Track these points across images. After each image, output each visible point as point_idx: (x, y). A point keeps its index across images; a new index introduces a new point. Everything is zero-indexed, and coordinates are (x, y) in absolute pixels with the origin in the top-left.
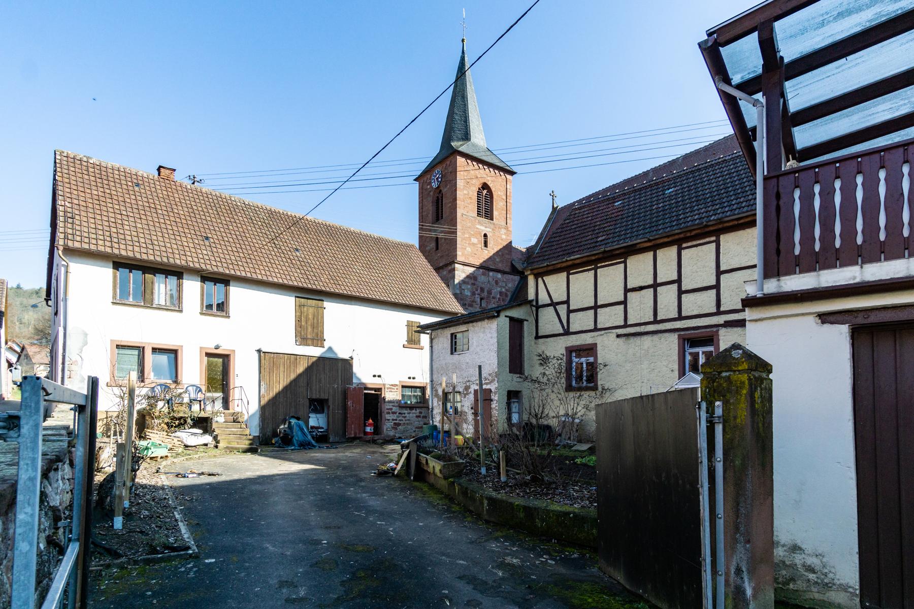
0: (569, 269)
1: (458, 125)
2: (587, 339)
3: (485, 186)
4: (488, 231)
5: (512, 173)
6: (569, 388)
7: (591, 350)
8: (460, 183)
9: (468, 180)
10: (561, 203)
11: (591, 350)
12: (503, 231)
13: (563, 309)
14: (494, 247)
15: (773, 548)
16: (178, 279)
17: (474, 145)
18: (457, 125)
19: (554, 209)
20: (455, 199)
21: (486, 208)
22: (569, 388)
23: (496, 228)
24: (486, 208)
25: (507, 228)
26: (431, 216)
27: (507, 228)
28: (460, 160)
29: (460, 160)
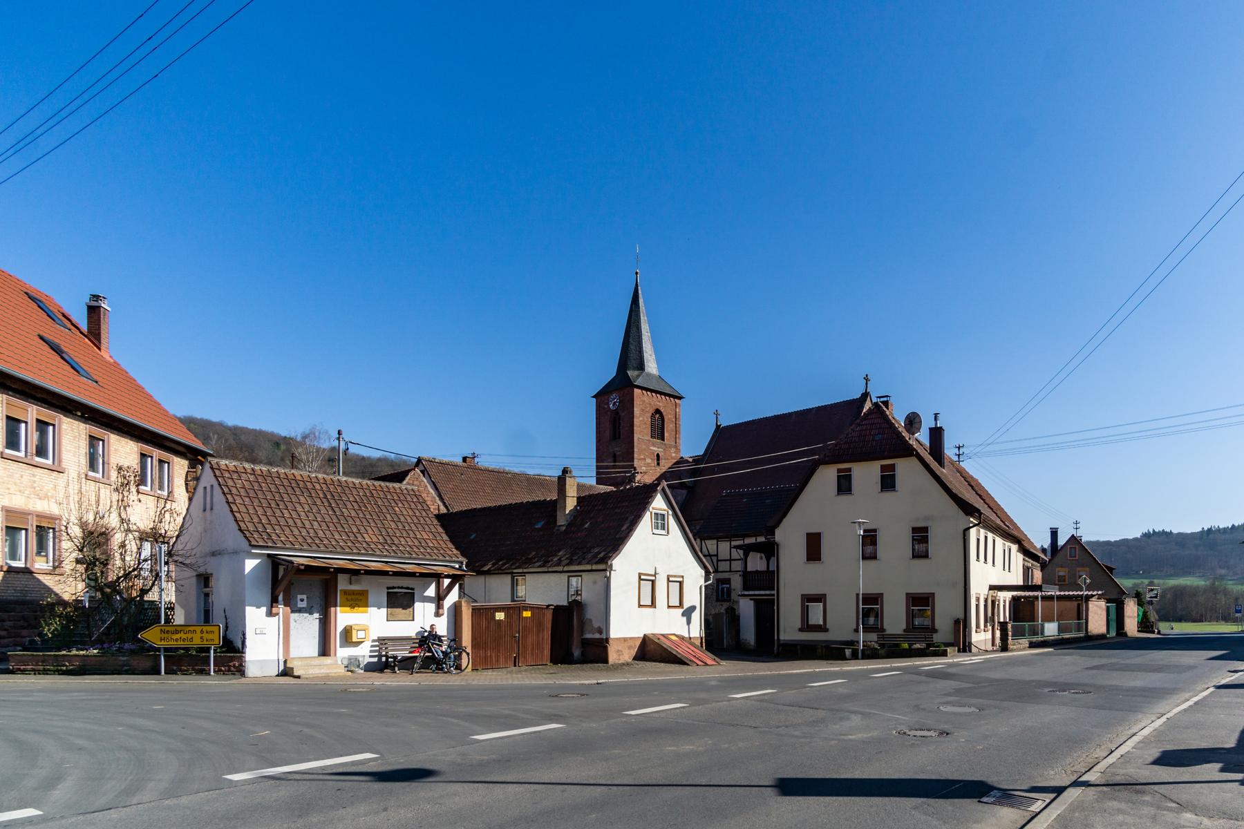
0: (718, 539)
1: (633, 355)
2: (726, 575)
3: (658, 411)
4: (660, 450)
5: (680, 398)
6: (717, 600)
7: (728, 581)
8: (637, 411)
9: (643, 405)
10: (724, 423)
11: (728, 581)
12: (673, 450)
13: (714, 559)
14: (665, 465)
15: (476, 469)
17: (649, 375)
18: (630, 355)
19: (718, 427)
20: (632, 425)
21: (658, 431)
22: (717, 600)
23: (666, 447)
24: (658, 431)
25: (676, 447)
26: (608, 434)
27: (676, 447)
28: (637, 391)
29: (637, 391)
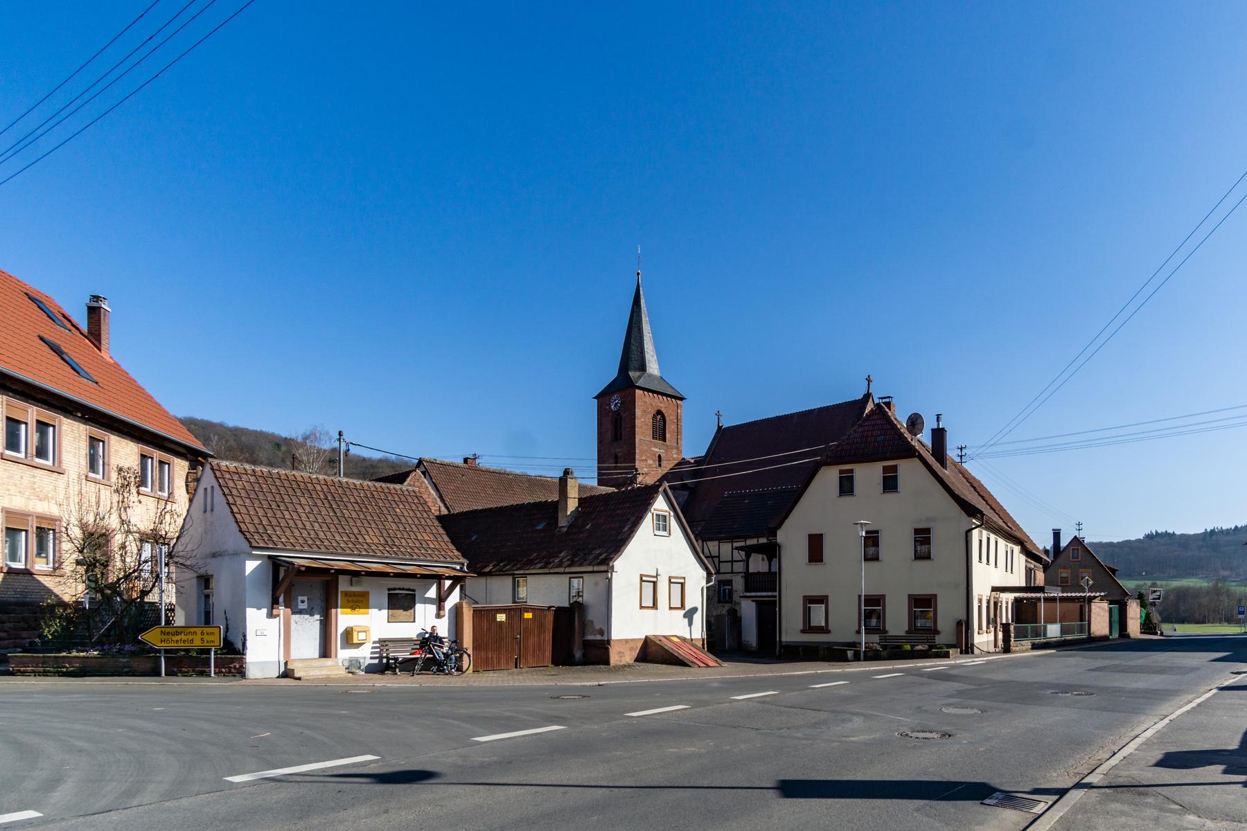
0: (720, 540)
1: (634, 356)
2: (728, 577)
3: (659, 412)
4: (661, 451)
5: (682, 399)
6: (719, 602)
7: (730, 582)
8: (638, 412)
9: (644, 406)
10: (726, 424)
11: (730, 582)
12: (674, 451)
13: (716, 560)
14: (667, 467)
15: (477, 470)
16: (193, 467)
17: (650, 376)
18: (632, 356)
19: (720, 428)
20: (634, 427)
21: (660, 432)
22: (719, 602)
23: (668, 449)
24: (660, 432)
25: (677, 448)
26: (609, 435)
27: (677, 448)
28: (638, 392)
29: (638, 392)
